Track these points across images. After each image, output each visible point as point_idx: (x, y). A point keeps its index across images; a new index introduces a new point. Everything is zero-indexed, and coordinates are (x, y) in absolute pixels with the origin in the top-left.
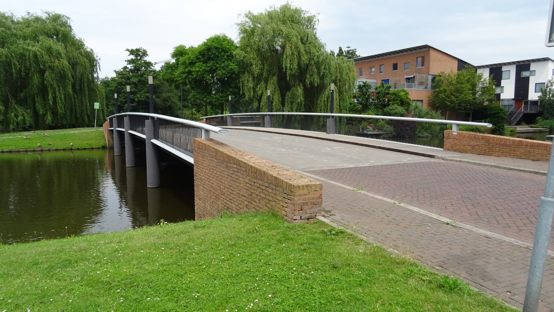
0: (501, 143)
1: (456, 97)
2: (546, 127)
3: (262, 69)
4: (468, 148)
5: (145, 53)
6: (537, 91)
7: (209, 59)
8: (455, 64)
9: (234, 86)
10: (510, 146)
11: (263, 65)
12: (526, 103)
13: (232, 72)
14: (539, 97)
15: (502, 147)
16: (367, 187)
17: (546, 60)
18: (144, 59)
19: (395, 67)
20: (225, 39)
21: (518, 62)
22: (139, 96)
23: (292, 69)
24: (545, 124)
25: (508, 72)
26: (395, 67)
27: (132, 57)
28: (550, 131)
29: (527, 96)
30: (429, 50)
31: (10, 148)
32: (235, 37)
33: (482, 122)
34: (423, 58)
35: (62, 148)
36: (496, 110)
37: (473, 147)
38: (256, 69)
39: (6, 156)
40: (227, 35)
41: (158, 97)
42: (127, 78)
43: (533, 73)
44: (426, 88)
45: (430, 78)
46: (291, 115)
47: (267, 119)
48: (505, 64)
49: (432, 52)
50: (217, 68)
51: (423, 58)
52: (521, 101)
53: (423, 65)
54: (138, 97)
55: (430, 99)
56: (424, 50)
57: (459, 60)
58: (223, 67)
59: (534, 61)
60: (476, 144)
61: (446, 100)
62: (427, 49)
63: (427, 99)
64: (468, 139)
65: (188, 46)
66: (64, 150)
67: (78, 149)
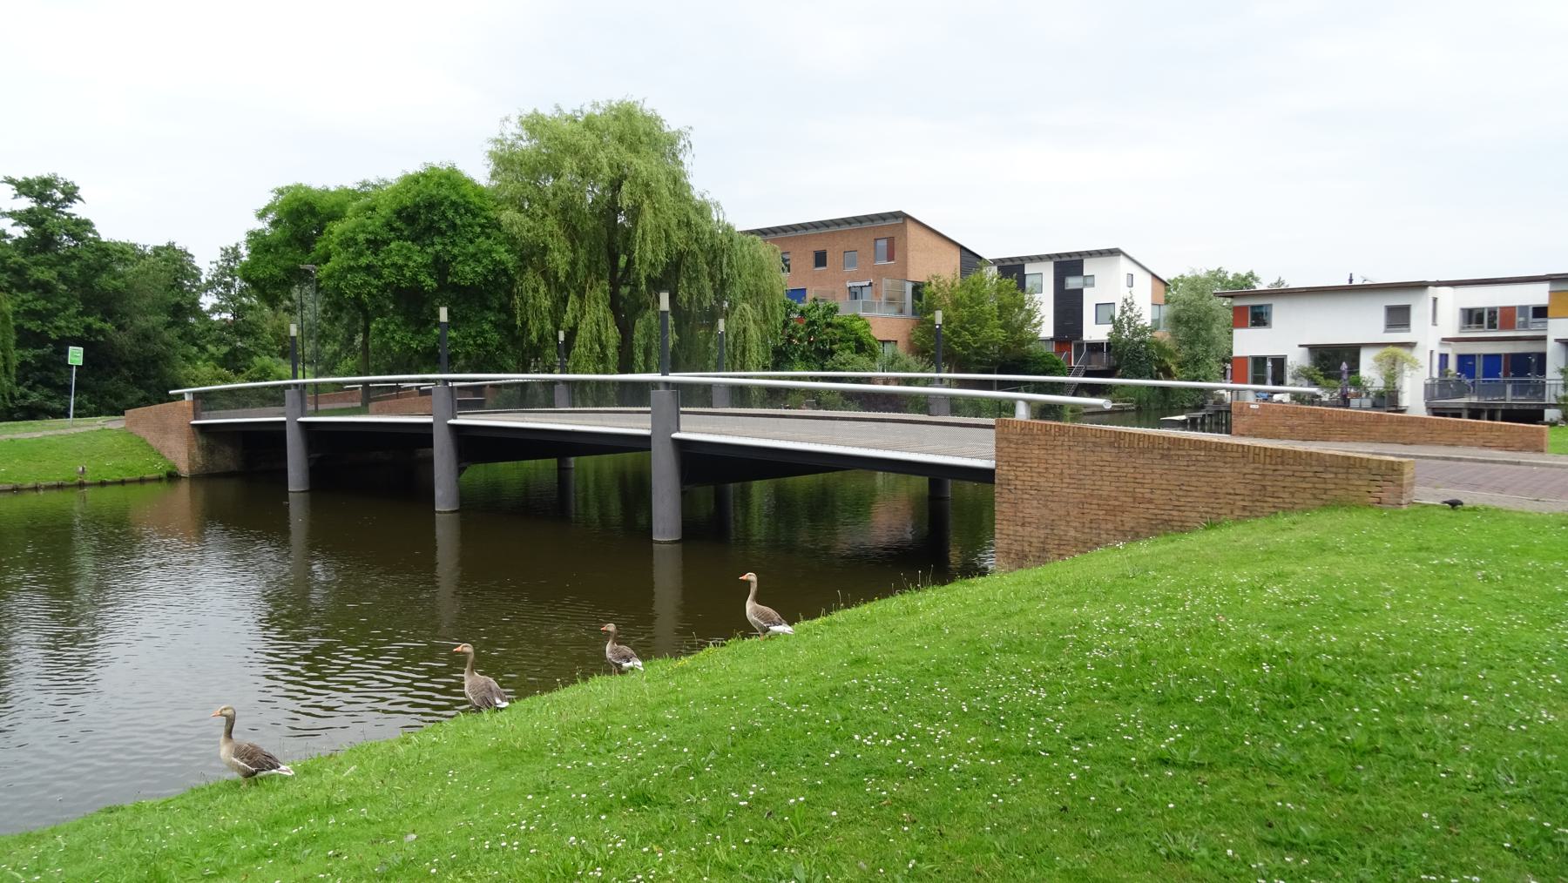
0: (1345, 419)
1: (973, 334)
2: (1131, 401)
3: (573, 263)
4: (1283, 430)
5: (71, 194)
6: (1099, 322)
7: (431, 229)
8: (955, 258)
9: (496, 304)
10: (1362, 423)
11: (574, 251)
12: (1080, 346)
13: (500, 270)
14: (1109, 334)
15: (1346, 425)
16: (287, 626)
17: (1114, 252)
18: (67, 210)
19: (820, 259)
20: (451, 179)
21: (1059, 255)
22: (63, 323)
23: (654, 264)
24: (1127, 395)
25: (1039, 277)
26: (820, 259)
27: (25, 203)
28: (1137, 408)
29: (1081, 333)
30: (904, 223)
31: (48, 483)
32: (479, 171)
33: (1021, 391)
34: (891, 241)
35: (54, 483)
36: (1046, 363)
37: (1292, 429)
38: (560, 260)
39: (18, 503)
40: (459, 167)
41: (120, 328)
42: (16, 266)
43: (1089, 281)
44: (901, 312)
45: (909, 287)
46: (605, 383)
47: (560, 393)
48: (1031, 259)
49: (910, 227)
50: (455, 257)
51: (891, 241)
52: (1069, 342)
53: (891, 257)
54: (57, 328)
55: (912, 338)
56: (894, 222)
57: (962, 248)
58: (474, 255)
59: (1090, 254)
60: (1297, 422)
61: (951, 340)
62: (900, 221)
63: (905, 339)
64: (1281, 415)
65: (1202, 273)
66: (60, 487)
67: (103, 484)
